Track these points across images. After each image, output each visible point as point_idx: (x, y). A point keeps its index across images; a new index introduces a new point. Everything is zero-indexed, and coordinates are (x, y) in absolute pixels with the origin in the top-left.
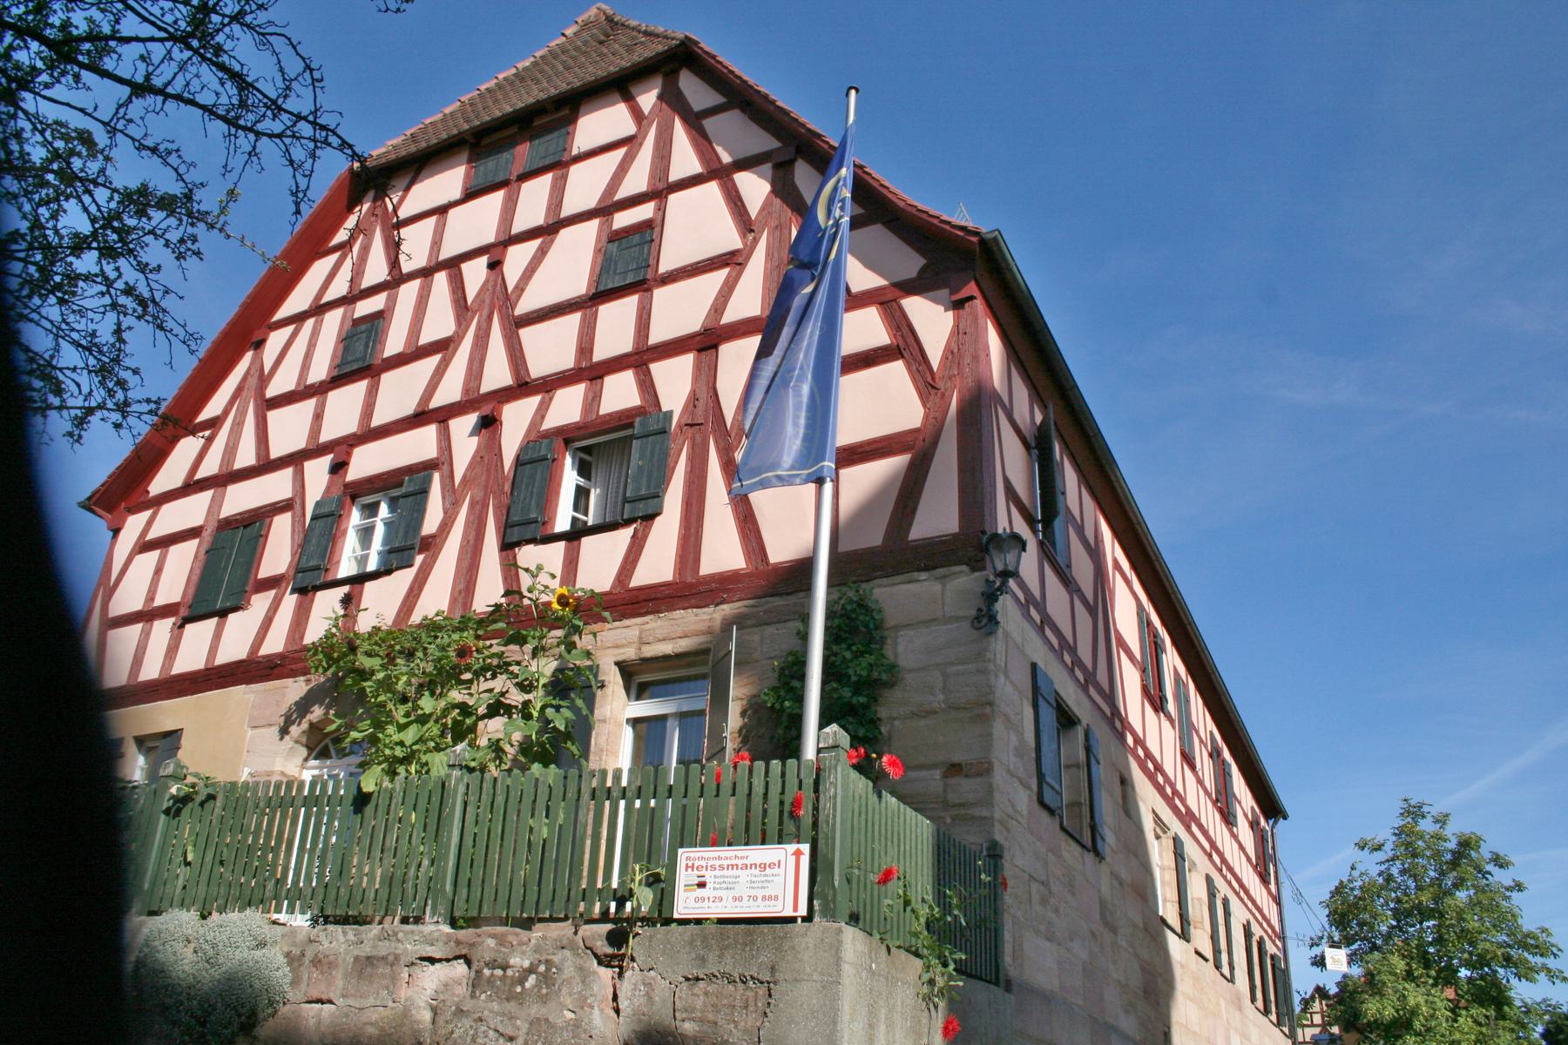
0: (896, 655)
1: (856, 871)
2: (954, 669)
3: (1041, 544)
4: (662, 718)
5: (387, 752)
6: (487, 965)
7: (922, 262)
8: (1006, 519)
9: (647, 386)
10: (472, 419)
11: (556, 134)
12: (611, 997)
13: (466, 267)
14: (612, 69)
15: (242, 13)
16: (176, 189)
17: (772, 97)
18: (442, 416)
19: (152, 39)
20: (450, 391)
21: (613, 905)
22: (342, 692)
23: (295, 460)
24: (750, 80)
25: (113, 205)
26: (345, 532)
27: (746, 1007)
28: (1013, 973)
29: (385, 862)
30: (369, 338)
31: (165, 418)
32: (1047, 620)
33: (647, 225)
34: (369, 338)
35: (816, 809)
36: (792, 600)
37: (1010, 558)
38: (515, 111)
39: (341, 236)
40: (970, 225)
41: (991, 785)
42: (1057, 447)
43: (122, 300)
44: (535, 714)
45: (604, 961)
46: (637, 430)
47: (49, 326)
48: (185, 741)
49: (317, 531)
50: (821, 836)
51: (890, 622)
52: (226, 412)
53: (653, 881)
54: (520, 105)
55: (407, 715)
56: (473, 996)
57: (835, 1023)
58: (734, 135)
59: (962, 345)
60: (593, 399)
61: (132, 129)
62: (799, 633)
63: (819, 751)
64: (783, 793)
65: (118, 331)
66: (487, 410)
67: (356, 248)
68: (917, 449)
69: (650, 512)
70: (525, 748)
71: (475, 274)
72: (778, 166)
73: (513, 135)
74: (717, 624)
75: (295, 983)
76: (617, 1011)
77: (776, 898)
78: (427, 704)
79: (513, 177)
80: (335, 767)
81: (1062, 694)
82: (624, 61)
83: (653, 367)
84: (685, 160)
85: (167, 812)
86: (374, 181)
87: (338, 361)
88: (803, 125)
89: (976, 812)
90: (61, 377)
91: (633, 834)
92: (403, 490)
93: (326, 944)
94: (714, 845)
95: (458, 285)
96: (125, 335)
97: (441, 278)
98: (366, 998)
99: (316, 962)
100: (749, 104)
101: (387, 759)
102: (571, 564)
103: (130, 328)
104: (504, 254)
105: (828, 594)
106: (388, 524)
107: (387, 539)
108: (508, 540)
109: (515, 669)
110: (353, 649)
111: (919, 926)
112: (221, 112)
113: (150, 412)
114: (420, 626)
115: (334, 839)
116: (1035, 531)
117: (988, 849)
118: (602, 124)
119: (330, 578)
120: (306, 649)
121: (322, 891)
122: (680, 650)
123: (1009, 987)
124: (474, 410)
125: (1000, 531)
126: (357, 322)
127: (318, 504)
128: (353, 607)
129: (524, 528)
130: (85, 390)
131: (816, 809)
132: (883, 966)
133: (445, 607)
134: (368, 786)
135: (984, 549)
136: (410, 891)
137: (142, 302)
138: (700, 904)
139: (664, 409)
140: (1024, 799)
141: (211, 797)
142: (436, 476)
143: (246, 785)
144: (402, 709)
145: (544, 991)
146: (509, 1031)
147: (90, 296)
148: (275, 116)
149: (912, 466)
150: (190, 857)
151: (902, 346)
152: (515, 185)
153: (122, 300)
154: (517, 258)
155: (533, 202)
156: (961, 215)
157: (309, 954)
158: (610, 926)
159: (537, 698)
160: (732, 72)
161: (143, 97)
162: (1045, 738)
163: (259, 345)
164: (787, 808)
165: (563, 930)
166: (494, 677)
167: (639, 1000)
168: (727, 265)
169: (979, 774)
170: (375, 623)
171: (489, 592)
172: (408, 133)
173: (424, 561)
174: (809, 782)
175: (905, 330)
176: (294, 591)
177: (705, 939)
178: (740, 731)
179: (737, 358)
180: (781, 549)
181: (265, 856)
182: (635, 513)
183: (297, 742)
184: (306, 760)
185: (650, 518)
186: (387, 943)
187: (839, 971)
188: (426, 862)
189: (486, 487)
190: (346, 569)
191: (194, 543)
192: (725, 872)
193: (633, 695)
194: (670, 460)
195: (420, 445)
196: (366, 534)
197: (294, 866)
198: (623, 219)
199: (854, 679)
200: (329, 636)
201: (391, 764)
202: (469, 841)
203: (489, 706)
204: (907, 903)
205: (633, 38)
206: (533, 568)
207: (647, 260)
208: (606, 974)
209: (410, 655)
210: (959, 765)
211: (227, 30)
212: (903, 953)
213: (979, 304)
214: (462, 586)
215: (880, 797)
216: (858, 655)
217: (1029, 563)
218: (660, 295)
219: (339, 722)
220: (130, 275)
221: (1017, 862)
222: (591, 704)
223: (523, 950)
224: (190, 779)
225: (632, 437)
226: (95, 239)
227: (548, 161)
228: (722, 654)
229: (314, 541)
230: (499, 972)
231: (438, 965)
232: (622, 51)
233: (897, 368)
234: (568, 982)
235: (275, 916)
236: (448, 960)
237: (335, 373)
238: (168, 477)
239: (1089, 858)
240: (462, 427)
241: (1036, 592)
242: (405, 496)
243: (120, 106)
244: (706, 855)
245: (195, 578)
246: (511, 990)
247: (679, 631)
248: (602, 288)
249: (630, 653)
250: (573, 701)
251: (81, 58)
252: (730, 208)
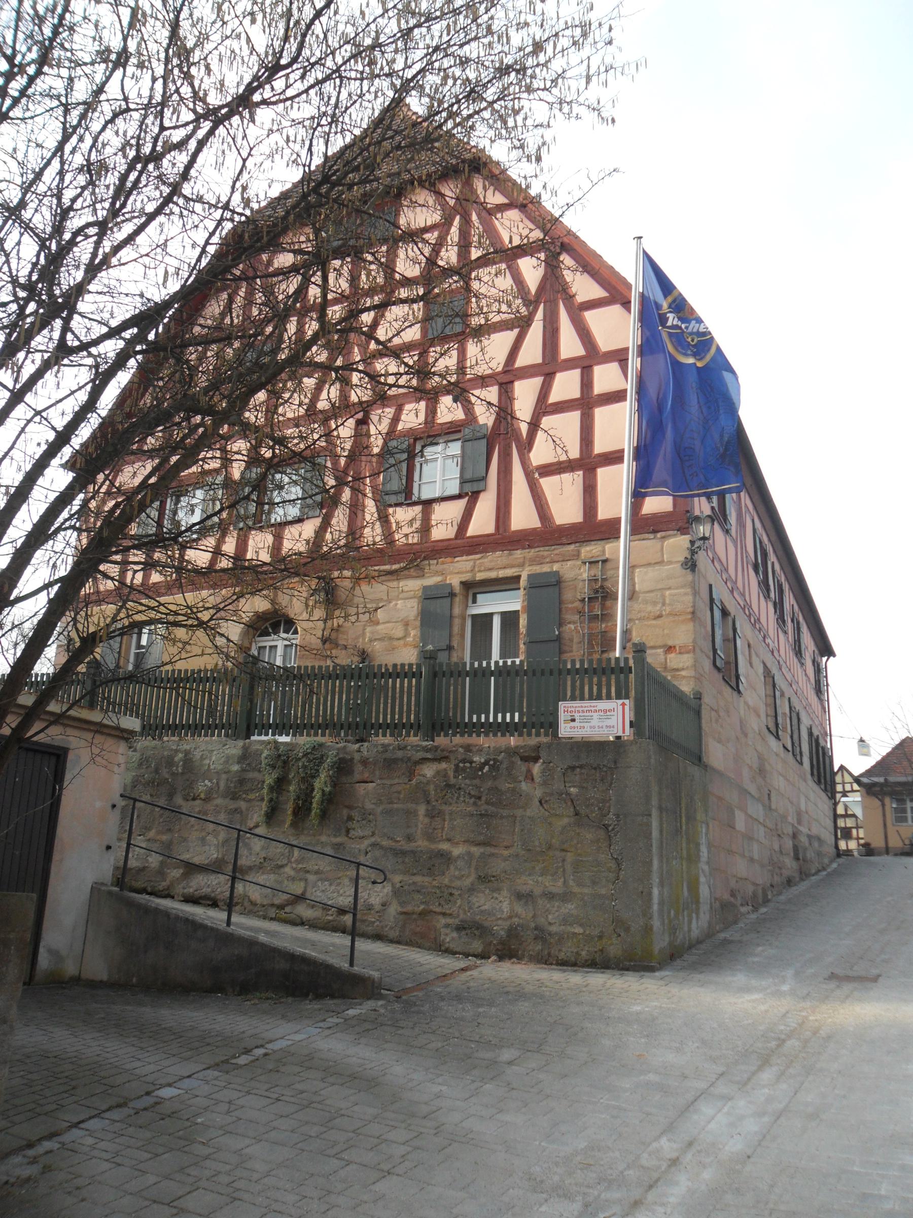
230: (468, 765)
239: (735, 693)
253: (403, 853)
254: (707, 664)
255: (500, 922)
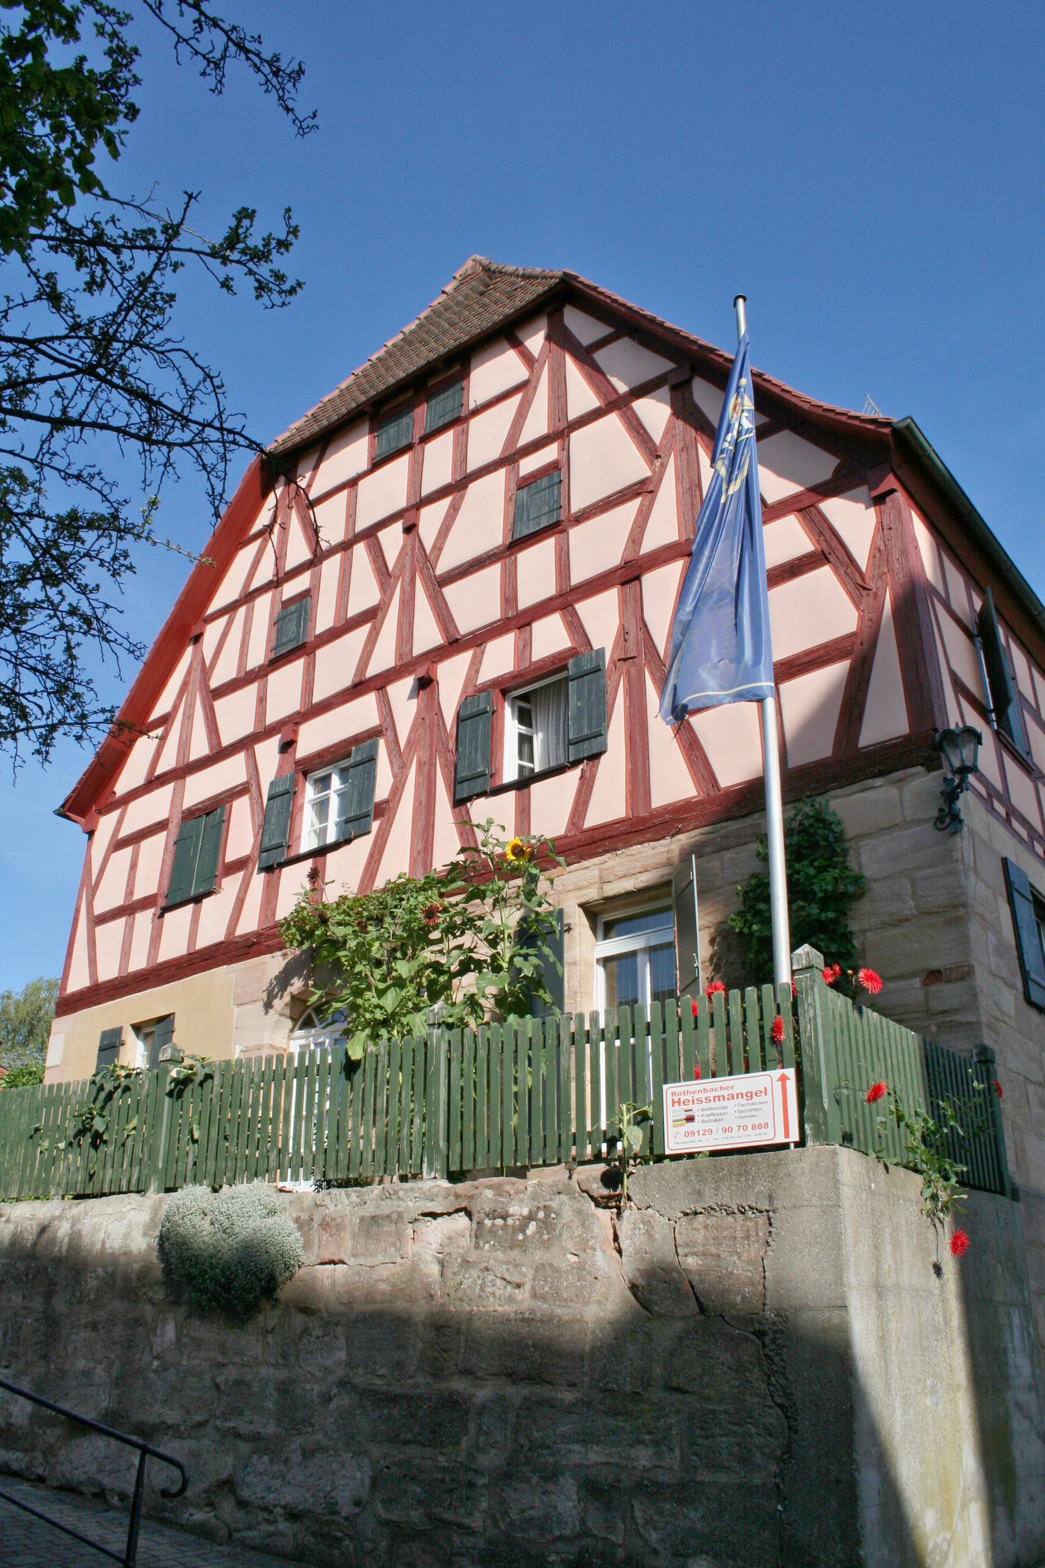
0: (860, 868)
1: (845, 1091)
2: (921, 874)
3: (997, 734)
4: (633, 954)
5: (368, 1016)
6: (487, 1215)
7: (838, 461)
8: (958, 714)
9: (575, 626)
10: (408, 683)
11: (450, 392)
12: (611, 1237)
13: (381, 535)
14: (496, 318)
15: (140, 335)
16: (104, 510)
17: (660, 319)
18: (380, 683)
19: (64, 375)
20: (383, 659)
21: (604, 1147)
22: (320, 964)
23: (246, 744)
24: (635, 305)
25: (49, 533)
26: (301, 808)
27: (748, 1238)
28: (1019, 1180)
29: (378, 1123)
30: (299, 617)
31: (120, 725)
32: (1012, 813)
33: (554, 467)
34: (299, 617)
35: (797, 1031)
36: (748, 821)
37: (967, 752)
38: (408, 375)
39: (263, 518)
40: (880, 416)
41: (974, 988)
42: (1001, 632)
43: (68, 620)
44: (505, 965)
45: (601, 1203)
46: (571, 671)
47: (8, 657)
48: (177, 1025)
49: (275, 811)
50: (805, 1059)
51: (848, 835)
52: (176, 708)
53: (642, 1119)
54: (412, 369)
55: (383, 979)
56: (477, 1247)
57: (839, 1247)
58: (627, 363)
59: (889, 543)
60: (524, 647)
61: (57, 462)
62: (758, 854)
63: (793, 973)
64: (761, 1019)
65: (69, 649)
66: (421, 672)
67: (274, 537)
68: (858, 654)
69: (595, 752)
70: (500, 1000)
71: (392, 539)
72: (674, 389)
73: (411, 398)
74: (675, 854)
75: (307, 1246)
76: (619, 1251)
77: (766, 1125)
78: (403, 968)
79: (416, 440)
80: (320, 1035)
81: (1038, 886)
82: (507, 309)
83: (579, 607)
84: (582, 396)
85: (170, 1094)
86: (280, 467)
87: (273, 644)
88: (695, 342)
89: (960, 1018)
90: (25, 702)
91: (616, 1075)
92: (351, 760)
93: (332, 1207)
94: (697, 1078)
95: (377, 554)
96: (74, 652)
97: (360, 549)
98: (376, 1256)
99: (325, 1225)
100: (637, 330)
101: (368, 1024)
102: (524, 813)
103: (78, 644)
104: (417, 517)
105: (784, 812)
106: (342, 795)
107: (343, 810)
108: (458, 797)
109: (479, 923)
110: (324, 921)
111: (915, 1141)
112: (133, 430)
113: (106, 721)
114: (384, 890)
115: (327, 1105)
116: (988, 722)
117: (979, 1055)
118: (495, 373)
119: (293, 853)
120: (278, 925)
121: (322, 1156)
122: (641, 885)
123: (1015, 1195)
124: (410, 674)
125: (952, 727)
126: (286, 604)
127: (272, 784)
128: (319, 881)
129: (471, 784)
130: (46, 709)
131: (797, 1031)
132: (882, 1185)
133: (406, 869)
134: (356, 1054)
135: (938, 748)
136: (406, 1150)
137: (86, 620)
138: (690, 1138)
139: (595, 648)
140: (1010, 1000)
141: (209, 1077)
142: (382, 743)
143: (239, 1062)
144: (378, 973)
145: (546, 1237)
146: (516, 1279)
147: (38, 622)
148: (183, 426)
149: (852, 672)
150: (196, 1135)
151: (827, 551)
152: (418, 448)
153: (68, 620)
154: (431, 518)
155: (438, 460)
156: (869, 408)
157: (317, 1219)
158: (602, 1167)
159: (506, 949)
160: (616, 301)
161: (63, 430)
162: (1024, 934)
163: (198, 639)
164: (768, 1033)
165: (556, 1174)
166: (463, 933)
167: (641, 1239)
168: (638, 494)
169: (962, 979)
170: (342, 892)
171: (447, 850)
172: (309, 414)
173: (380, 827)
174: (786, 1005)
175: (827, 533)
176: (261, 870)
177: (698, 1172)
178: (711, 959)
179: (661, 587)
180: (730, 775)
181: (263, 1130)
182: (582, 753)
183: (281, 1015)
184: (292, 1031)
185: (595, 757)
186: (389, 1201)
187: (837, 1194)
188: (417, 1121)
189: (431, 747)
190: (307, 843)
191: (162, 836)
192: (712, 1104)
193: (600, 933)
194: (609, 698)
195: (361, 715)
196: (322, 807)
197: (294, 1134)
198: (528, 465)
199: (820, 895)
200: (299, 910)
201: (373, 1028)
202: (456, 1096)
203: (461, 963)
204: (900, 1118)
205: (513, 284)
206: (483, 823)
207: (558, 501)
208: (605, 1215)
209: (379, 920)
210: (939, 972)
211: (129, 353)
212: (902, 1171)
213: (900, 496)
214: (420, 847)
215: (860, 1012)
216: (821, 870)
217: (987, 756)
218: (576, 534)
219: (319, 993)
220: (72, 597)
221: (1010, 1065)
222: (559, 952)
223: (521, 1196)
224: (187, 1062)
225: (567, 680)
226: (38, 569)
227: (447, 419)
228: (683, 885)
229: (273, 820)
230: (499, 1222)
231: (440, 1220)
232: (503, 298)
233: (825, 572)
234: (568, 1226)
235: (280, 1184)
236: (449, 1214)
237: (272, 656)
238: (128, 779)
240: (401, 690)
241: (998, 785)
242: (355, 766)
243: (43, 442)
244: (691, 1089)
245: (168, 869)
246: (513, 1238)
247: (638, 867)
248: (517, 536)
249: (592, 894)
250: (539, 949)
251: (4, 405)
252: (634, 438)
253: (392, 1399)
254: (1021, 997)
255: (560, 1545)
